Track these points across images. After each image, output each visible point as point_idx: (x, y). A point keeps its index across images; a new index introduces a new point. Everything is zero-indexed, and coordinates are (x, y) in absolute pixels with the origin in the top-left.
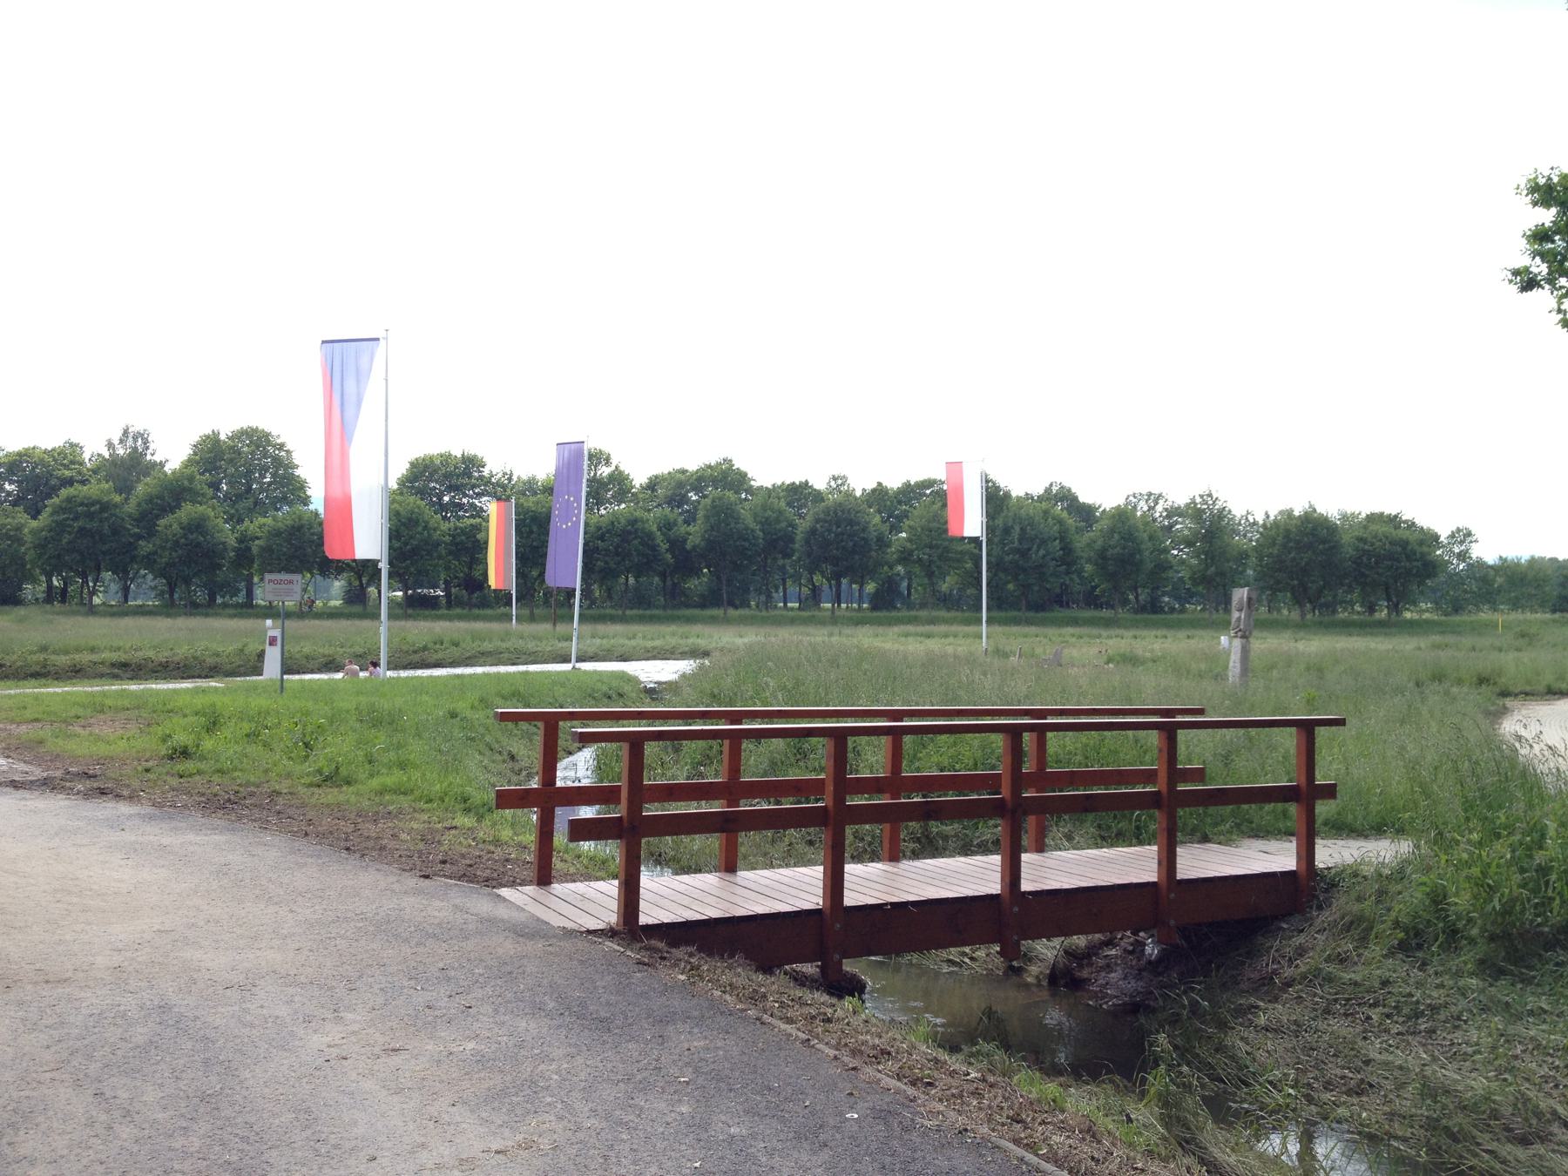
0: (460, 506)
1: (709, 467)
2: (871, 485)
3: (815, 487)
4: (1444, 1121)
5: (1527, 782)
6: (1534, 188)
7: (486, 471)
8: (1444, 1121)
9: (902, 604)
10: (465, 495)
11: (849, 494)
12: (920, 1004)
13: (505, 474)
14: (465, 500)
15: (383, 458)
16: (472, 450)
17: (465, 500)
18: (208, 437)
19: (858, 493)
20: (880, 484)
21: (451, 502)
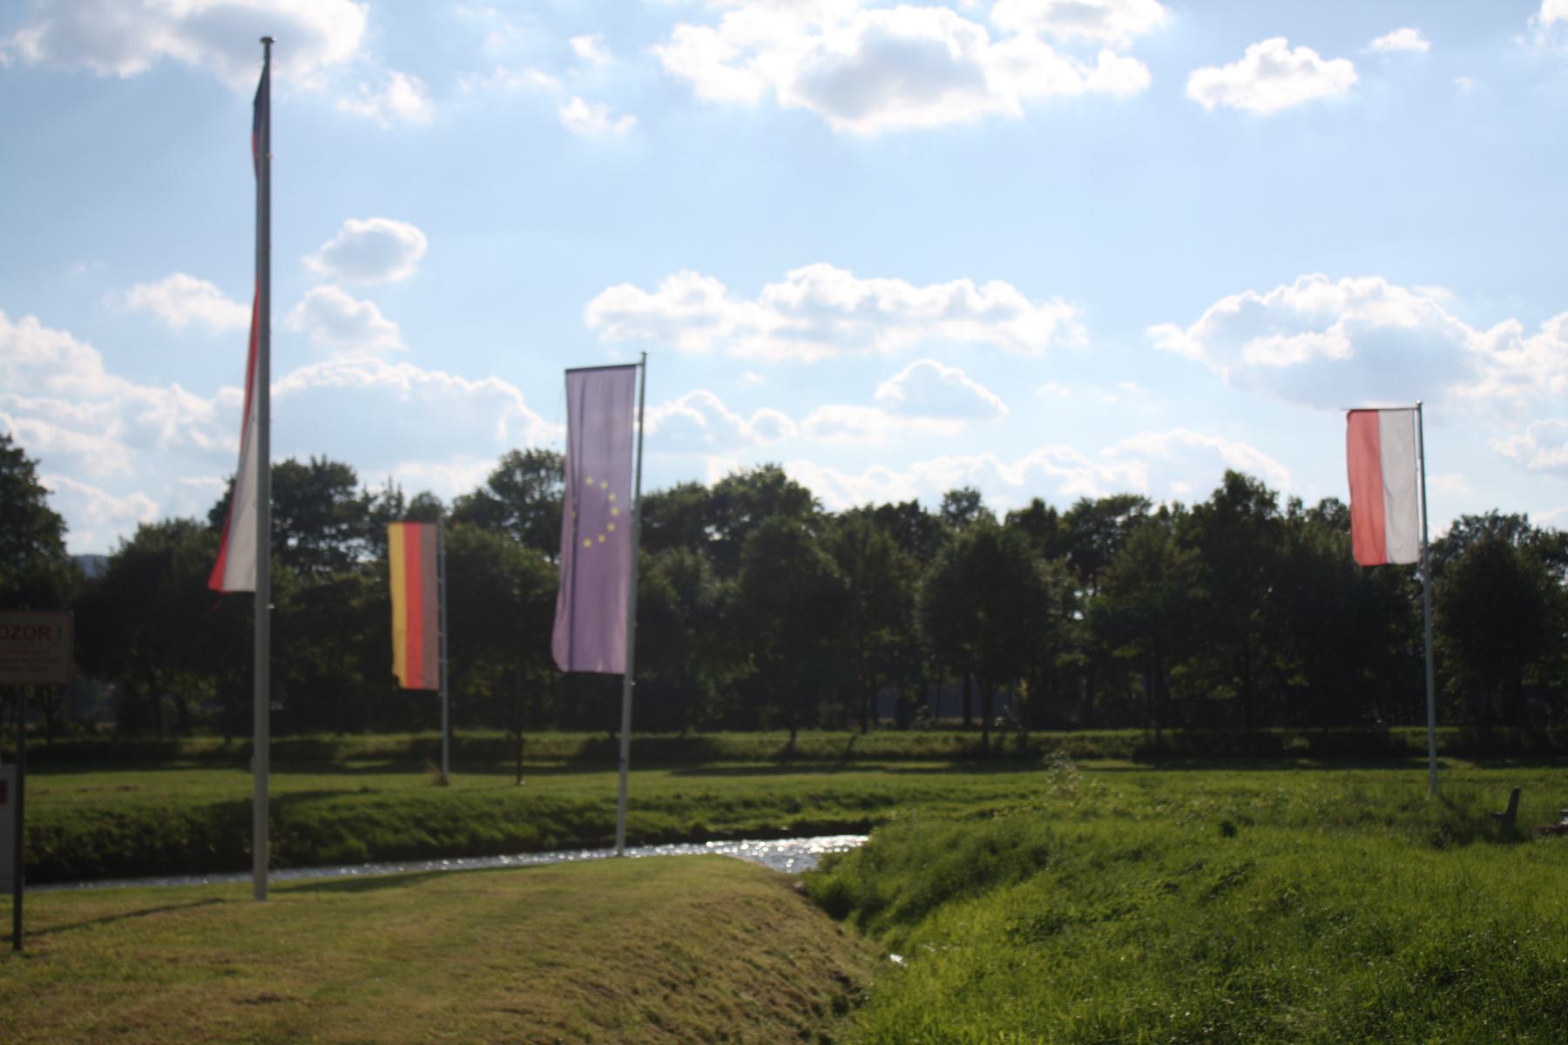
0: (316, 556)
1: (741, 481)
2: (1022, 503)
3: (1534, 523)
4: (1055, 912)
5: (1497, 896)
6: (1277, 493)
7: (358, 492)
8: (1055, 912)
9: (1239, 503)
10: (323, 537)
11: (130, 545)
12: (958, 720)
13: (390, 498)
14: (323, 545)
15: (1429, 523)
16: (336, 456)
17: (323, 545)
18: (1080, 505)
19: (1001, 520)
20: (1038, 505)
21: (300, 550)
